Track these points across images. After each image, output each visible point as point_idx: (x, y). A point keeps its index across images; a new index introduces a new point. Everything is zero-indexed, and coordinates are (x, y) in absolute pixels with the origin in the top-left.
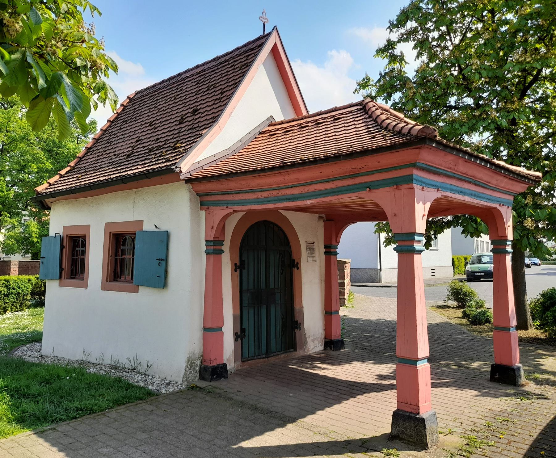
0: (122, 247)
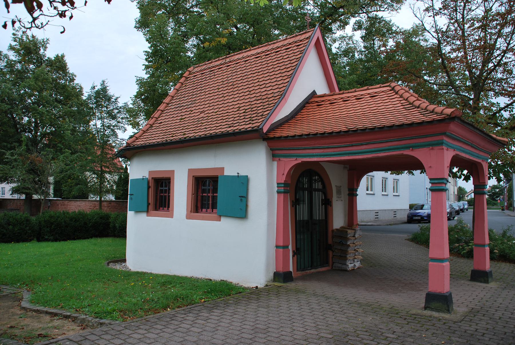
0: (160, 188)
